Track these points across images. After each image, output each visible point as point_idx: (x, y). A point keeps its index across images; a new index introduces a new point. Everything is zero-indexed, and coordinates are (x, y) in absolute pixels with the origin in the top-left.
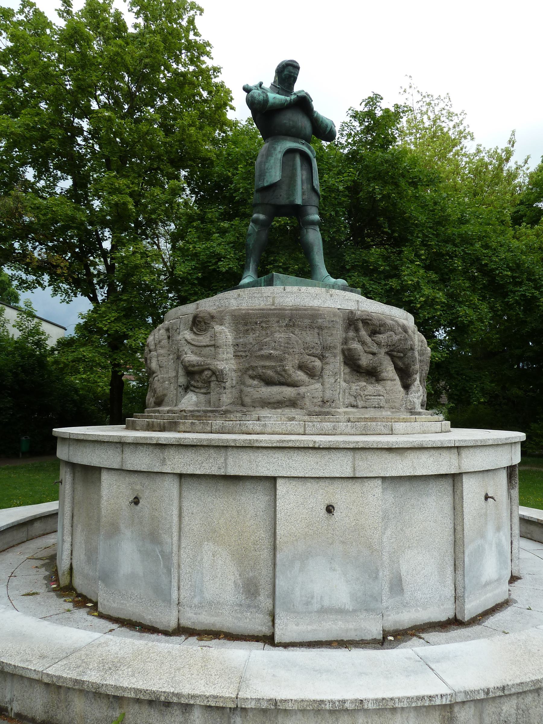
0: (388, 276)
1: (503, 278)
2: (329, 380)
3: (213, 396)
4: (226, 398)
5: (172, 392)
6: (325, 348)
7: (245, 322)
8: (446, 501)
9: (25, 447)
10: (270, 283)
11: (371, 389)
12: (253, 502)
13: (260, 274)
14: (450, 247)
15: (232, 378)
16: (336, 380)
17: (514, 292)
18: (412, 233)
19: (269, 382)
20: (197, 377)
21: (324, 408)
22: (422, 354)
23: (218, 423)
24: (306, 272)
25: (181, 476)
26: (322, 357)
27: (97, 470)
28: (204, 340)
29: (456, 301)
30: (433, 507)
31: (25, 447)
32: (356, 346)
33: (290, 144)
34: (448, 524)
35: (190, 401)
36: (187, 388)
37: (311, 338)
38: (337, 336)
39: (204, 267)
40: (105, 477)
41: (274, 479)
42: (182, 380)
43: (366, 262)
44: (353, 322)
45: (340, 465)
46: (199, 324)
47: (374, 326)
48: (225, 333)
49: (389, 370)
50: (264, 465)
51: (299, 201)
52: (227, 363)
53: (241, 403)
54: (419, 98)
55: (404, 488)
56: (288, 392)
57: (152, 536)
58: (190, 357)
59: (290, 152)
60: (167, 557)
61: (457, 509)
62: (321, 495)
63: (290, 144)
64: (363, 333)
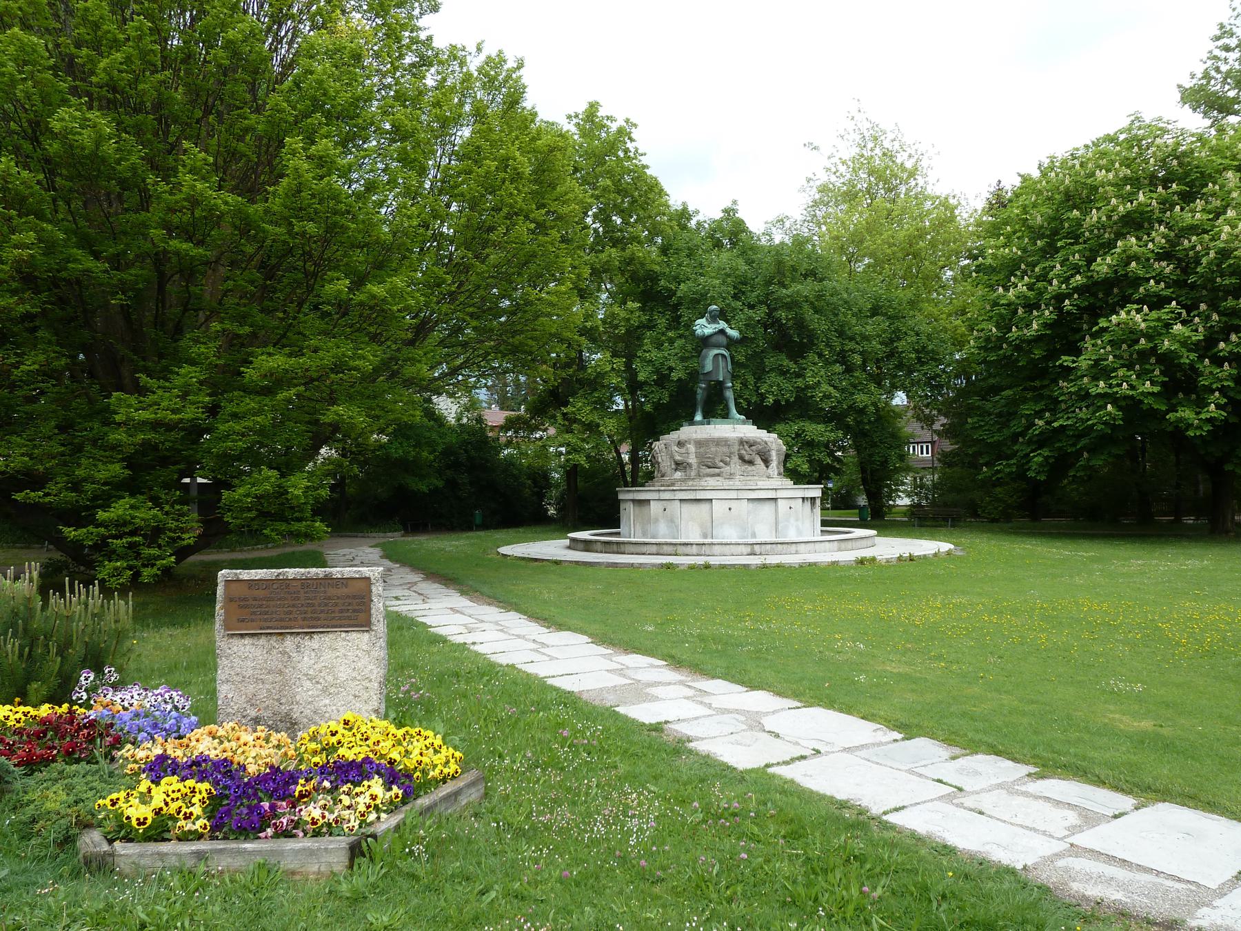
0: (798, 375)
7: (699, 443)
9: (478, 520)
11: (750, 468)
12: (705, 506)
13: (704, 417)
15: (695, 466)
16: (736, 466)
20: (679, 465)
21: (731, 476)
23: (690, 483)
24: (725, 415)
28: (683, 450)
30: (767, 508)
31: (478, 520)
33: (716, 351)
35: (678, 475)
37: (725, 449)
38: (736, 447)
39: (657, 371)
44: (742, 442)
45: (733, 495)
46: (680, 444)
47: (751, 444)
48: (692, 448)
49: (758, 460)
52: (693, 460)
53: (699, 475)
54: (869, 126)
56: (717, 471)
58: (678, 458)
62: (727, 504)
63: (716, 351)
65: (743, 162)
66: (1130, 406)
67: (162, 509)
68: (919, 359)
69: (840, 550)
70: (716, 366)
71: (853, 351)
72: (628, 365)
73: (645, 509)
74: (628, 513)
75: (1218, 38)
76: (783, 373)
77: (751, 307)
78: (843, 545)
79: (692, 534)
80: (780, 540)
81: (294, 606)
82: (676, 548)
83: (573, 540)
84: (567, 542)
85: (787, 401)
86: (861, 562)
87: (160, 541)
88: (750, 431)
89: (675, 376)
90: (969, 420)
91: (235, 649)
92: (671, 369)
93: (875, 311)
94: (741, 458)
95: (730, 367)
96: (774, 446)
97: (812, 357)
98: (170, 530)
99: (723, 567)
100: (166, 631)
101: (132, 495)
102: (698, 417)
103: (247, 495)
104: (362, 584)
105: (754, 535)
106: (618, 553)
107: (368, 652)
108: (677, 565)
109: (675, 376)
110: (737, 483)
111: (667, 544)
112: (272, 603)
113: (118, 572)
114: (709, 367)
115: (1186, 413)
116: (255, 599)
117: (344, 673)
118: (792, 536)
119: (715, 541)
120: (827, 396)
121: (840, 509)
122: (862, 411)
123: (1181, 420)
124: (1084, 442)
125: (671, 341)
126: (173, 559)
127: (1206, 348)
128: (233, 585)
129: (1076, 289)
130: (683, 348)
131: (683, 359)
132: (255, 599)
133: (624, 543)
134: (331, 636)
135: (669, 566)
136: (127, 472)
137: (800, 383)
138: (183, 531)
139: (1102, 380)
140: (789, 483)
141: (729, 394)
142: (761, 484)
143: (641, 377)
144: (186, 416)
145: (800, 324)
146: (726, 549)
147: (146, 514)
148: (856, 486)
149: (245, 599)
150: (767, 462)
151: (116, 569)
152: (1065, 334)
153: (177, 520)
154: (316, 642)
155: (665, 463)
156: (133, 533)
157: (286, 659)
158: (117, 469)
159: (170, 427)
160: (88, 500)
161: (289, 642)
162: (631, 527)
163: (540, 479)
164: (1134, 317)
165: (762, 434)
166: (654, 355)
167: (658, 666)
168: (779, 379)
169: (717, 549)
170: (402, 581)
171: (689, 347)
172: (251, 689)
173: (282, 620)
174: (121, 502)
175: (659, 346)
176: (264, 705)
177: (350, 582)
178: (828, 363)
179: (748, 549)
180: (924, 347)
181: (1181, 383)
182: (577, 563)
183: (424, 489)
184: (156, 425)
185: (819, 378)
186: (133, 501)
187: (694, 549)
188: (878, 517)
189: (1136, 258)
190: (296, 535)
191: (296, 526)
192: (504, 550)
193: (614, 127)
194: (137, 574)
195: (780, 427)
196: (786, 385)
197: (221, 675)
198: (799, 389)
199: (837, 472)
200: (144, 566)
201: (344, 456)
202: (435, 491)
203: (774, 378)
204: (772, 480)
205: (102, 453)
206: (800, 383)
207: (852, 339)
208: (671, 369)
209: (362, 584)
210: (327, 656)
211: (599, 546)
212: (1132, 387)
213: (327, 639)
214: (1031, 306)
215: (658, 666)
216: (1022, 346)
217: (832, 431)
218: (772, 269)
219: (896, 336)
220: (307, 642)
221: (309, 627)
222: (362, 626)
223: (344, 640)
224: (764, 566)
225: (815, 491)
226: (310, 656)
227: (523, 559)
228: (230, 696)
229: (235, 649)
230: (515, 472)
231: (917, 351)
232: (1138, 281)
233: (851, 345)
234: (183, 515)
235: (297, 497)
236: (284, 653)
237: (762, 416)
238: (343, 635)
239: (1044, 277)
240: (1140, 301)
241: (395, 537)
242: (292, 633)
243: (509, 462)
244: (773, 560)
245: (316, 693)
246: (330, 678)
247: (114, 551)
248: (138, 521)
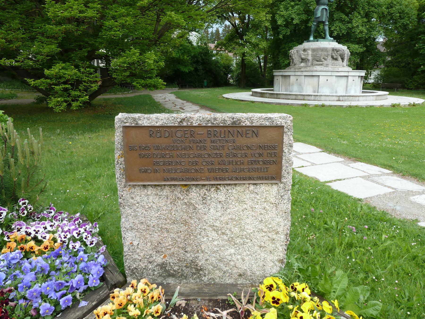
0: (348, 22)
1: (396, 17)
2: (328, 61)
3: (307, 64)
4: (310, 64)
5: (298, 63)
6: (328, 55)
7: (314, 50)
8: (346, 80)
9: (205, 84)
10: (317, 41)
12: (316, 79)
14: (373, 9)
15: (311, 60)
17: (399, 22)
18: (359, 6)
19: (318, 61)
20: (303, 60)
21: (327, 65)
22: (347, 54)
23: (309, 68)
24: (324, 38)
25: (305, 76)
26: (327, 56)
27: (290, 76)
28: (306, 53)
29: (372, 29)
30: (344, 80)
31: (205, 84)
32: (334, 54)
34: (346, 84)
35: (302, 64)
36: (301, 62)
37: (326, 53)
38: (330, 53)
39: (286, 20)
40: (291, 76)
41: (319, 76)
42: (300, 61)
43: (341, 18)
44: (333, 50)
45: (329, 74)
46: (305, 50)
47: (337, 50)
48: (310, 52)
49: (340, 58)
50: (318, 74)
51: (324, 20)
52: (310, 58)
55: (339, 78)
56: (321, 63)
57: (300, 85)
58: (303, 57)
59: (323, 9)
60: (302, 88)
61: (347, 81)
62: (326, 78)
64: (335, 52)
67: (79, 71)
68: (400, 16)
69: (376, 100)
70: (322, 15)
71: (373, 12)
72: (273, 17)
73: (287, 80)
74: (279, 82)
76: (342, 21)
78: (378, 98)
79: (308, 90)
80: (347, 95)
81: (200, 156)
82: (304, 97)
83: (253, 92)
84: (251, 93)
85: (343, 34)
87: (80, 88)
88: (335, 45)
89: (295, 22)
90: (417, 45)
91: (138, 198)
92: (292, 19)
94: (333, 57)
95: (328, 15)
96: (346, 52)
97: (356, 14)
98: (85, 82)
99: (331, 106)
100: (87, 135)
101: (64, 62)
102: (311, 38)
103: (124, 63)
104: (274, 134)
105: (336, 92)
106: (277, 98)
107: (276, 205)
108: (309, 105)
109: (295, 22)
110: (330, 68)
111: (300, 95)
112: (174, 153)
113: (59, 104)
114: (319, 15)
116: (158, 148)
117: (250, 225)
118: (352, 93)
119: (319, 94)
120: (361, 32)
125: (293, 7)
126: (87, 97)
128: (133, 132)
131: (298, 14)
132: (158, 148)
133: (280, 94)
134: (238, 188)
135: (306, 105)
136: (59, 49)
137: (350, 25)
138: (92, 82)
140: (350, 69)
142: (340, 69)
143: (279, 22)
144: (88, 15)
146: (327, 98)
147: (71, 72)
149: (146, 148)
151: (58, 102)
153: (88, 77)
154: (221, 195)
156: (65, 83)
157: (191, 210)
158: (54, 48)
159: (79, 21)
160: (40, 65)
161: (195, 195)
162: (279, 87)
163: (227, 68)
166: (284, 13)
167: (388, 174)
168: (340, 24)
169: (323, 98)
170: (191, 110)
171: (302, 9)
172: (156, 237)
173: (187, 171)
174: (58, 65)
175: (287, 9)
176: (169, 252)
177: (261, 131)
178: (362, 17)
179: (337, 98)
180: (403, 11)
182: (262, 102)
183: (187, 71)
184: (69, 20)
186: (63, 65)
187: (313, 98)
190: (146, 86)
191: (149, 81)
192: (226, 96)
194: (70, 105)
196: (344, 27)
197: (125, 223)
200: (73, 101)
202: (190, 72)
203: (337, 23)
204: (344, 68)
205: (46, 39)
206: (350, 25)
207: (372, 6)
208: (292, 19)
209: (274, 134)
210: (234, 208)
211: (268, 95)
213: (235, 191)
215: (388, 174)
217: (361, 48)
220: (213, 194)
221: (216, 179)
222: (273, 178)
223: (252, 192)
224: (350, 107)
226: (216, 208)
227: (236, 100)
228: (135, 243)
229: (138, 198)
230: (219, 65)
231: (400, 13)
234: (91, 74)
235: (149, 64)
236: (189, 204)
237: (338, 39)
238: (252, 187)
241: (176, 90)
242: (197, 185)
243: (217, 62)
244: (354, 103)
245: (221, 243)
246: (236, 230)
247: (57, 93)
248: (66, 76)
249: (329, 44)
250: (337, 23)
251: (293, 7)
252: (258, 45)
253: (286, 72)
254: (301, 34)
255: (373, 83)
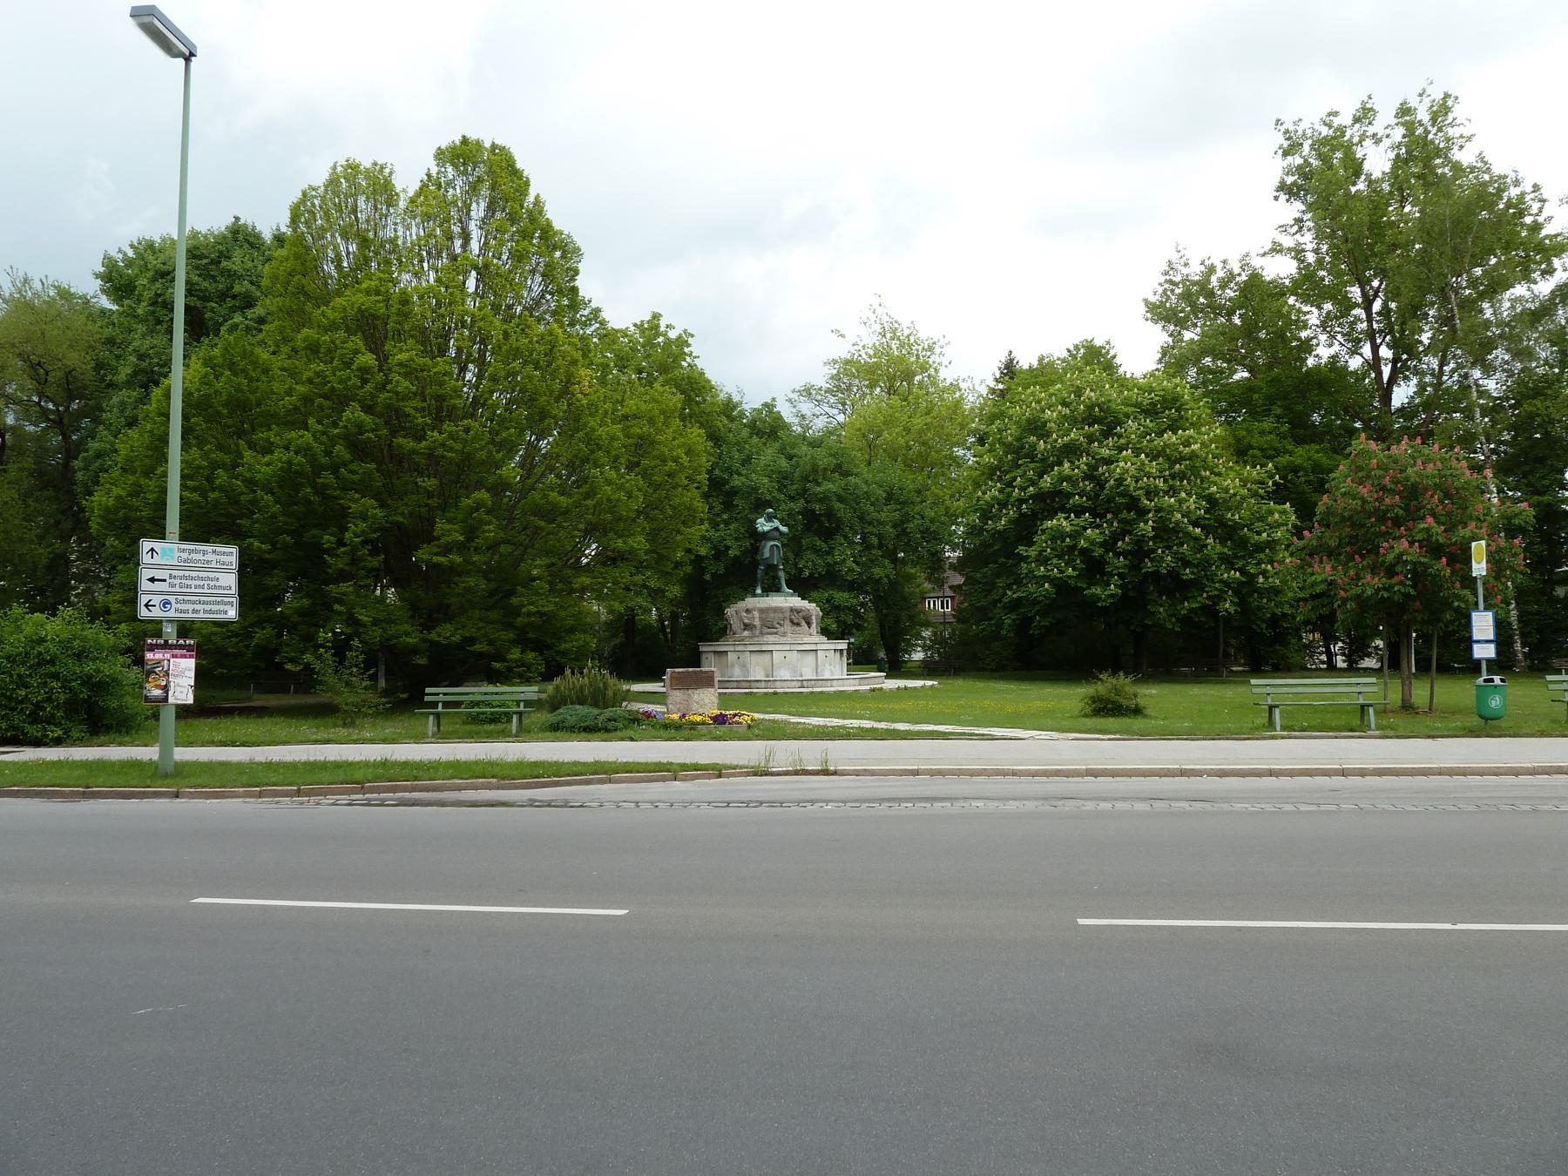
0: (828, 553)
7: (761, 611)
12: (768, 656)
16: (788, 626)
20: (747, 627)
21: (784, 634)
24: (778, 590)
30: (811, 657)
35: (746, 633)
39: (715, 547)
44: (792, 610)
46: (748, 611)
47: (798, 611)
48: (756, 614)
52: (757, 623)
53: (762, 633)
57: (744, 666)
65: (775, 348)
66: (1061, 585)
75: (1166, 273)
76: (816, 551)
77: (792, 498)
86: (873, 690)
88: (796, 602)
92: (728, 548)
93: (890, 497)
102: (759, 591)
110: (789, 639)
114: (767, 554)
115: (1097, 590)
120: (851, 570)
121: (860, 659)
122: (878, 581)
123: (1094, 595)
124: (1037, 608)
125: (727, 523)
127: (1109, 545)
129: (1031, 497)
130: (736, 530)
131: (737, 539)
139: (1042, 571)
140: (824, 639)
141: (782, 574)
142: (806, 640)
145: (830, 514)
148: (878, 640)
150: (809, 624)
152: (1025, 528)
155: (735, 624)
164: (1061, 522)
165: (805, 604)
168: (813, 556)
181: (1094, 568)
185: (845, 556)
188: (895, 668)
189: (1068, 479)
193: (673, 335)
195: (814, 594)
198: (828, 565)
199: (859, 627)
201: (48, 568)
203: (809, 555)
206: (829, 560)
207: (870, 523)
208: (728, 548)
212: (1061, 572)
214: (1003, 505)
216: (999, 535)
218: (808, 467)
219: (906, 518)
225: (843, 645)
232: (1070, 495)
233: (870, 529)
237: (801, 586)
239: (1010, 484)
240: (1069, 511)
249: (788, 601)
250: (809, 555)
251: (727, 523)
252: (663, 591)
253: (721, 647)
254: (747, 573)
255: (923, 661)
